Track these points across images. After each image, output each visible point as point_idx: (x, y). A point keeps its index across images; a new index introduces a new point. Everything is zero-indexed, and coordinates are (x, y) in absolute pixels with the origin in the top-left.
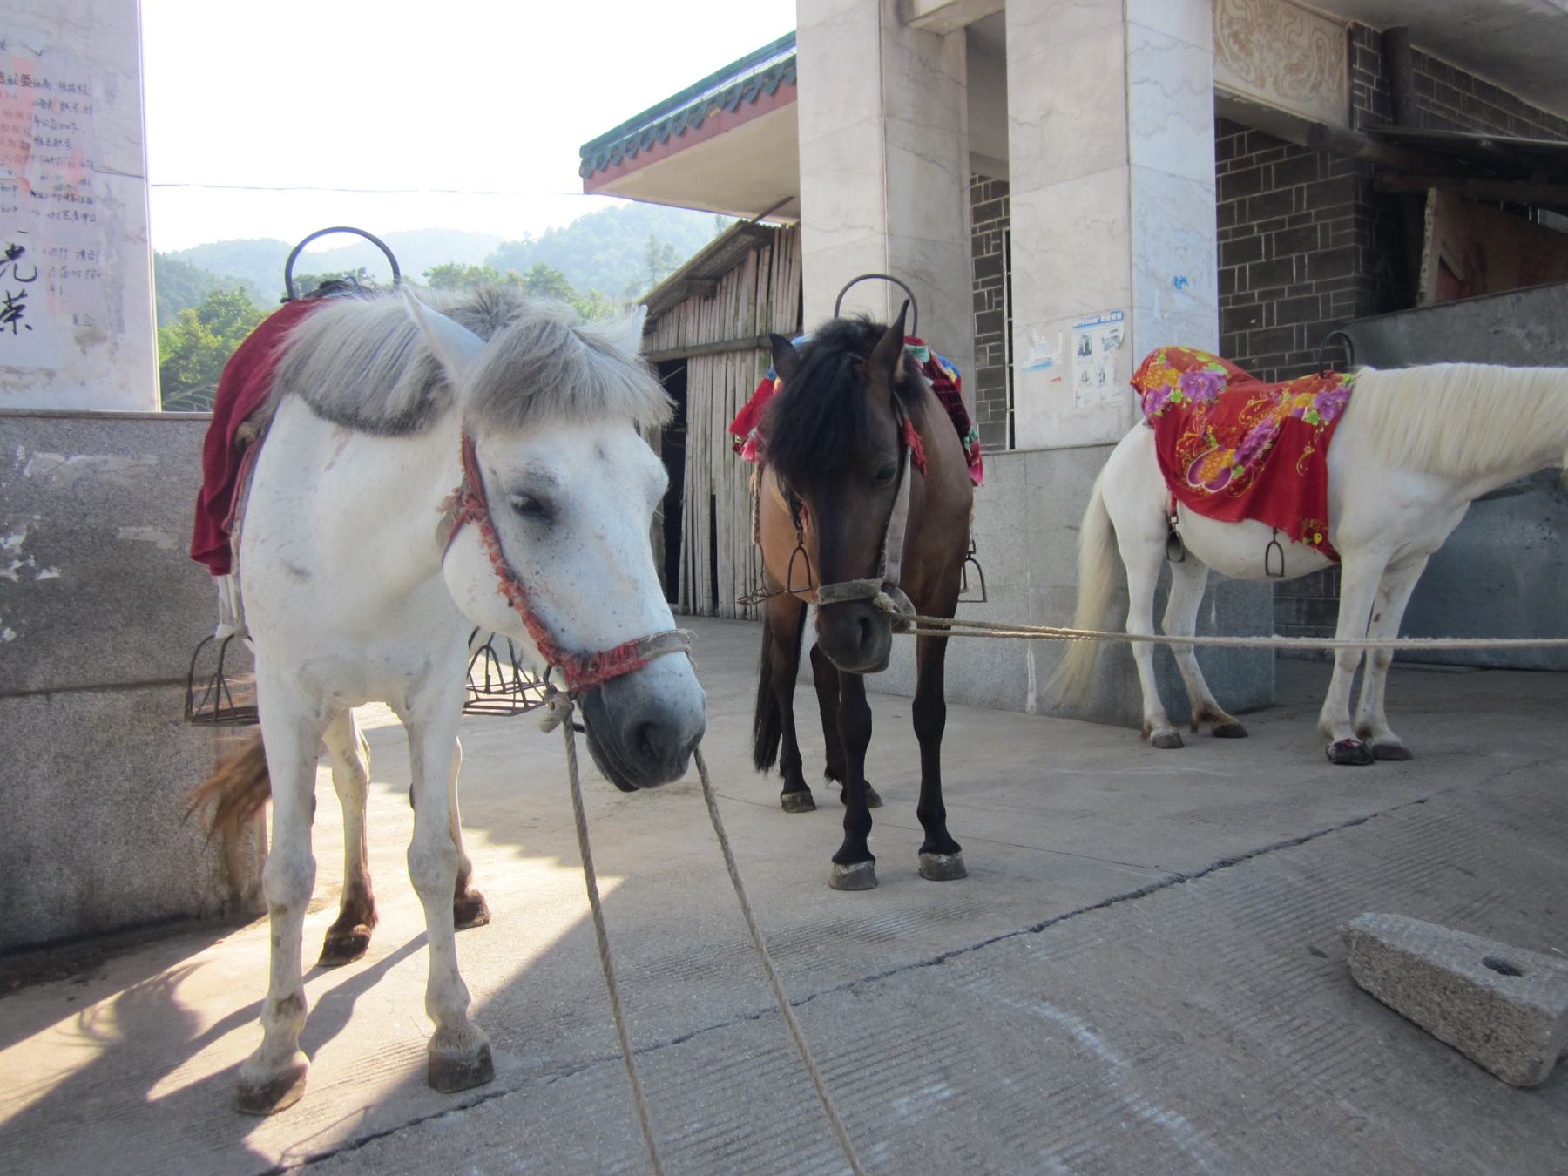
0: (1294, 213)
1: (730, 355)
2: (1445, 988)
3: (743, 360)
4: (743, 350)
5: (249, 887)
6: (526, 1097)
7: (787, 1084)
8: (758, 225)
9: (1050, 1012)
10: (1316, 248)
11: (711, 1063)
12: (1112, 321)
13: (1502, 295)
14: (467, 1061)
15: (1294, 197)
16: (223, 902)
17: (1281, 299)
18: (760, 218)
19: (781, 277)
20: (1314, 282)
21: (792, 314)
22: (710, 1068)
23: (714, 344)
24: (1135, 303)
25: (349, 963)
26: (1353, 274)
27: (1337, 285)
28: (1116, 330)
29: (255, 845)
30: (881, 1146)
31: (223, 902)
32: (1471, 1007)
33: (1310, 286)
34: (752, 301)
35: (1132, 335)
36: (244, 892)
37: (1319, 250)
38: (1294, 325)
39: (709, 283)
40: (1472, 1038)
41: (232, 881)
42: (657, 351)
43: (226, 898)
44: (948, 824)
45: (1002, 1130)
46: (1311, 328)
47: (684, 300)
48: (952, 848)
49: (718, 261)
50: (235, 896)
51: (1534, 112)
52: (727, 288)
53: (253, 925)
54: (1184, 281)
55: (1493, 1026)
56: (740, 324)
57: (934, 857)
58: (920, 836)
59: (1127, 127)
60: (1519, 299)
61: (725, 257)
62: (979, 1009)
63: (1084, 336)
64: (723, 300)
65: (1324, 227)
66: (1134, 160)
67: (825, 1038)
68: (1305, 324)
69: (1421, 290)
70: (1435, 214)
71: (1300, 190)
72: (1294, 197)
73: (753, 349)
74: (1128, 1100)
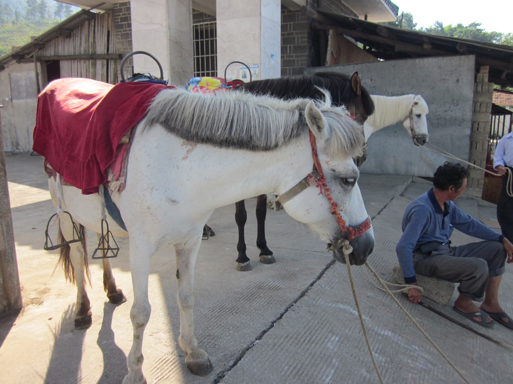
0: (288, 32)
1: (79, 60)
2: (425, 282)
3: (84, 63)
4: (85, 59)
5: (14, 299)
6: (235, 371)
7: (299, 347)
8: (90, 12)
9: (341, 306)
10: (295, 44)
11: (275, 345)
12: (254, 67)
13: (350, 65)
14: (206, 363)
15: (289, 27)
16: (5, 307)
17: (284, 59)
18: (91, 9)
19: (99, 32)
20: (294, 55)
21: (105, 47)
22: (276, 347)
23: (71, 55)
24: (262, 63)
25: (90, 326)
26: (306, 53)
27: (302, 56)
28: (255, 71)
29: (15, 282)
30: (334, 360)
31: (5, 307)
32: (432, 286)
33: (293, 56)
34: (87, 40)
35: (261, 73)
36: (13, 302)
37: (296, 45)
38: (288, 68)
39: (68, 31)
40: (432, 294)
41: (8, 298)
42: (46, 56)
43: (6, 305)
44: (268, 245)
45: (356, 347)
46: (293, 69)
47: (57, 37)
48: (271, 253)
49: (72, 23)
50: (9, 304)
51: (344, 5)
52: (76, 34)
53: (20, 315)
54: (273, 55)
55: (438, 291)
56: (82, 49)
57: (266, 257)
58: (259, 251)
59: (260, 2)
60: (355, 66)
61: (75, 22)
62: (325, 309)
63: (244, 72)
64: (74, 38)
65: (298, 38)
66: (263, 14)
67: (297, 328)
68: (291, 68)
69: (327, 61)
70: (331, 38)
71: (290, 25)
72: (289, 27)
73: (89, 59)
74: (376, 330)
